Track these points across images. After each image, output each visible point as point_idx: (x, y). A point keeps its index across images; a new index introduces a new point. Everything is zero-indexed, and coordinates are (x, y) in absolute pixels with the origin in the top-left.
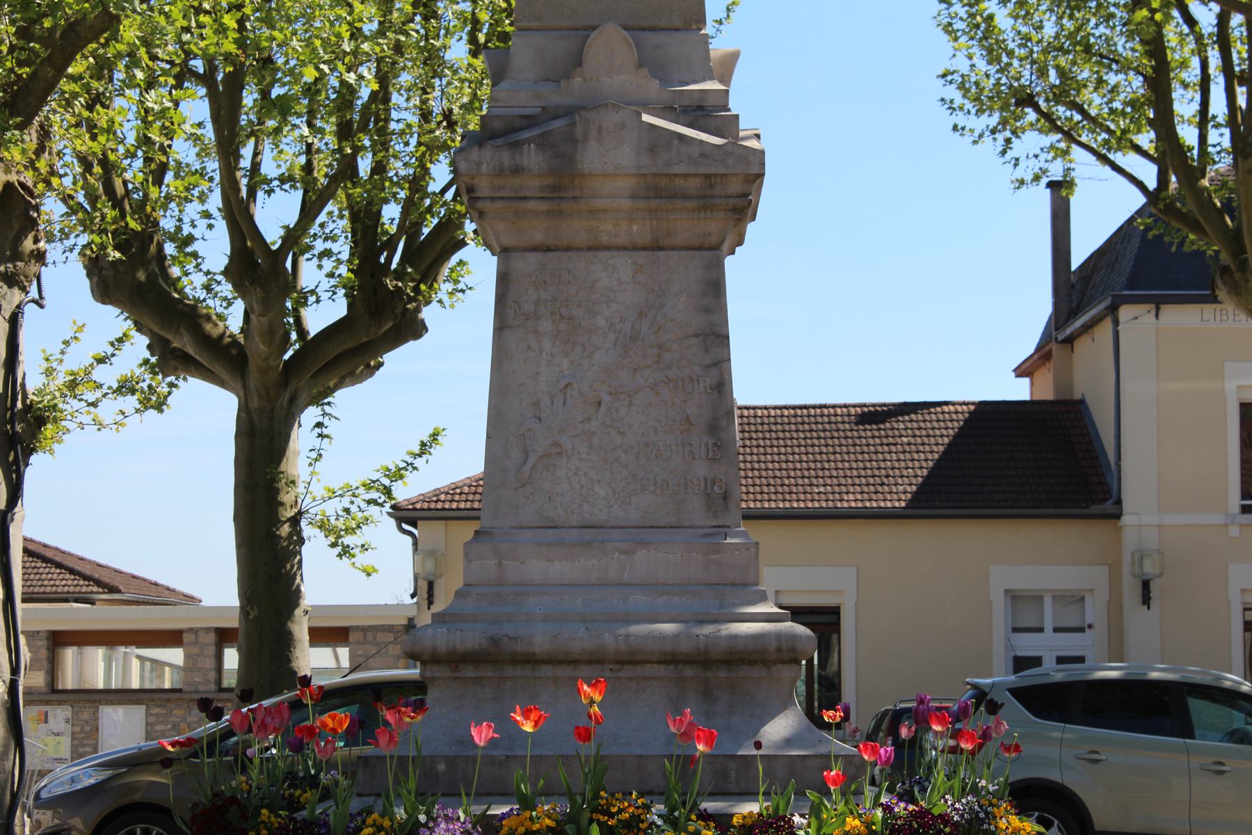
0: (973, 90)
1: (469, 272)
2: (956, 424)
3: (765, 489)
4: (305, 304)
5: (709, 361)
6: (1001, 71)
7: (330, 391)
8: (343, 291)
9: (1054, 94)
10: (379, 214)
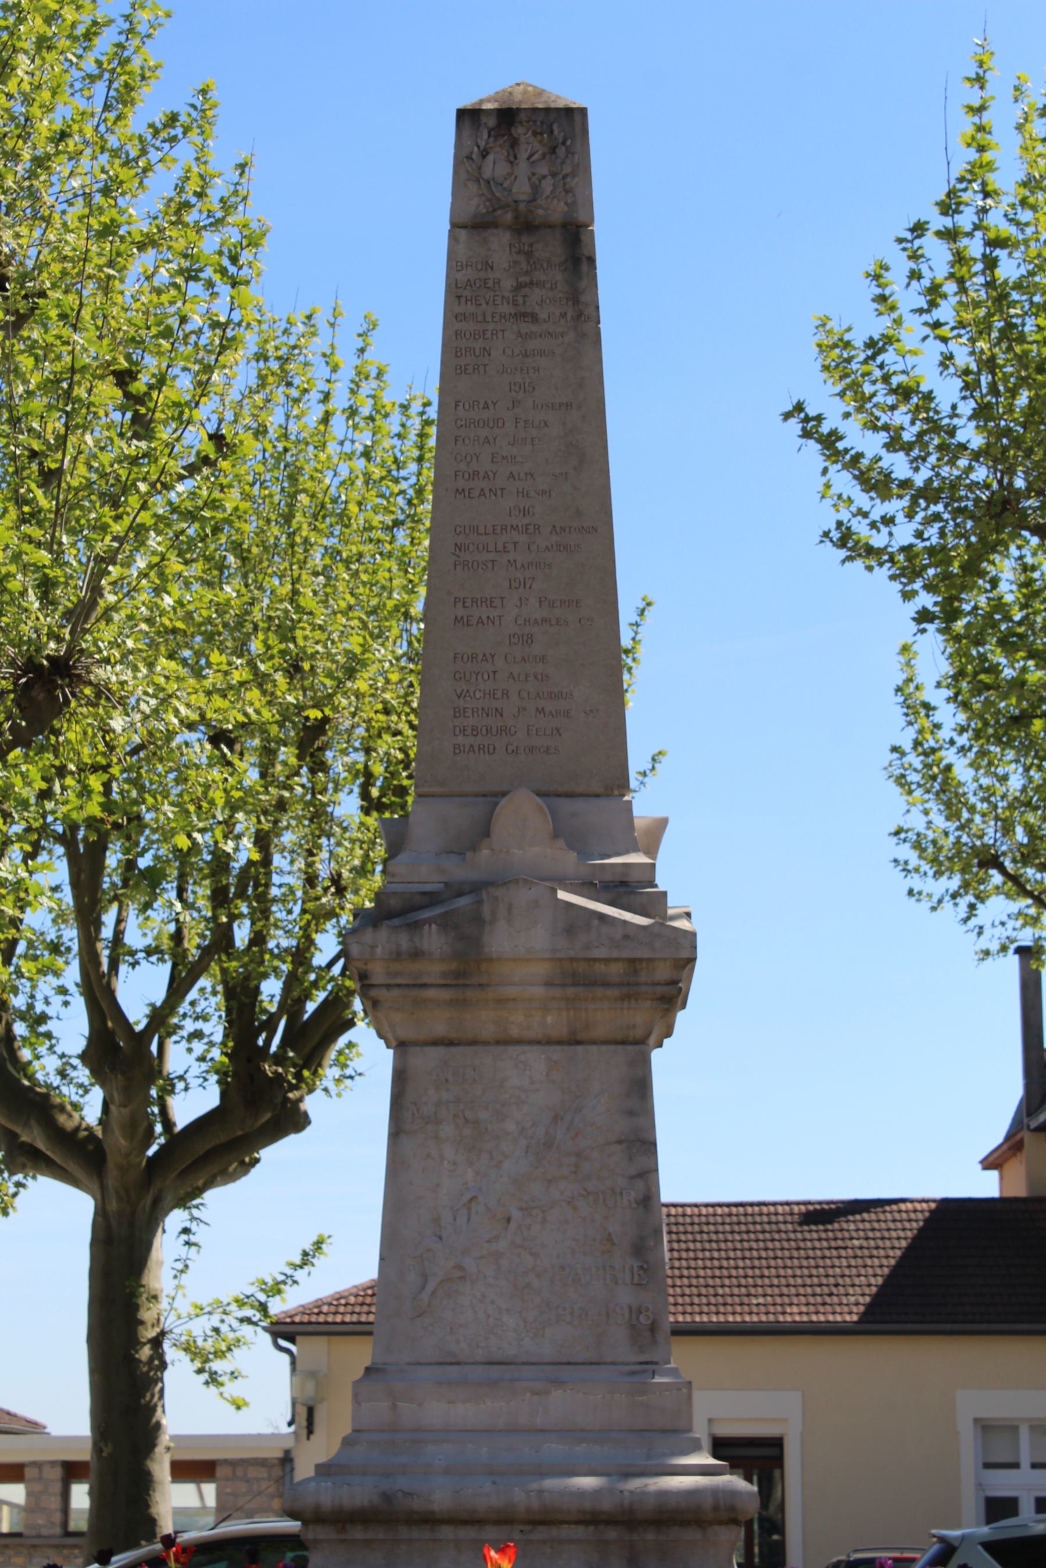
0: (930, 850)
1: (359, 1055)
2: (914, 1225)
3: (696, 1300)
4: (172, 1092)
5: (633, 1171)
6: (961, 828)
7: (199, 1192)
8: (215, 1077)
9: (1022, 854)
10: (257, 991)
